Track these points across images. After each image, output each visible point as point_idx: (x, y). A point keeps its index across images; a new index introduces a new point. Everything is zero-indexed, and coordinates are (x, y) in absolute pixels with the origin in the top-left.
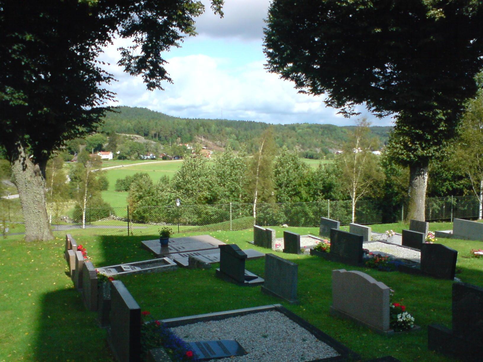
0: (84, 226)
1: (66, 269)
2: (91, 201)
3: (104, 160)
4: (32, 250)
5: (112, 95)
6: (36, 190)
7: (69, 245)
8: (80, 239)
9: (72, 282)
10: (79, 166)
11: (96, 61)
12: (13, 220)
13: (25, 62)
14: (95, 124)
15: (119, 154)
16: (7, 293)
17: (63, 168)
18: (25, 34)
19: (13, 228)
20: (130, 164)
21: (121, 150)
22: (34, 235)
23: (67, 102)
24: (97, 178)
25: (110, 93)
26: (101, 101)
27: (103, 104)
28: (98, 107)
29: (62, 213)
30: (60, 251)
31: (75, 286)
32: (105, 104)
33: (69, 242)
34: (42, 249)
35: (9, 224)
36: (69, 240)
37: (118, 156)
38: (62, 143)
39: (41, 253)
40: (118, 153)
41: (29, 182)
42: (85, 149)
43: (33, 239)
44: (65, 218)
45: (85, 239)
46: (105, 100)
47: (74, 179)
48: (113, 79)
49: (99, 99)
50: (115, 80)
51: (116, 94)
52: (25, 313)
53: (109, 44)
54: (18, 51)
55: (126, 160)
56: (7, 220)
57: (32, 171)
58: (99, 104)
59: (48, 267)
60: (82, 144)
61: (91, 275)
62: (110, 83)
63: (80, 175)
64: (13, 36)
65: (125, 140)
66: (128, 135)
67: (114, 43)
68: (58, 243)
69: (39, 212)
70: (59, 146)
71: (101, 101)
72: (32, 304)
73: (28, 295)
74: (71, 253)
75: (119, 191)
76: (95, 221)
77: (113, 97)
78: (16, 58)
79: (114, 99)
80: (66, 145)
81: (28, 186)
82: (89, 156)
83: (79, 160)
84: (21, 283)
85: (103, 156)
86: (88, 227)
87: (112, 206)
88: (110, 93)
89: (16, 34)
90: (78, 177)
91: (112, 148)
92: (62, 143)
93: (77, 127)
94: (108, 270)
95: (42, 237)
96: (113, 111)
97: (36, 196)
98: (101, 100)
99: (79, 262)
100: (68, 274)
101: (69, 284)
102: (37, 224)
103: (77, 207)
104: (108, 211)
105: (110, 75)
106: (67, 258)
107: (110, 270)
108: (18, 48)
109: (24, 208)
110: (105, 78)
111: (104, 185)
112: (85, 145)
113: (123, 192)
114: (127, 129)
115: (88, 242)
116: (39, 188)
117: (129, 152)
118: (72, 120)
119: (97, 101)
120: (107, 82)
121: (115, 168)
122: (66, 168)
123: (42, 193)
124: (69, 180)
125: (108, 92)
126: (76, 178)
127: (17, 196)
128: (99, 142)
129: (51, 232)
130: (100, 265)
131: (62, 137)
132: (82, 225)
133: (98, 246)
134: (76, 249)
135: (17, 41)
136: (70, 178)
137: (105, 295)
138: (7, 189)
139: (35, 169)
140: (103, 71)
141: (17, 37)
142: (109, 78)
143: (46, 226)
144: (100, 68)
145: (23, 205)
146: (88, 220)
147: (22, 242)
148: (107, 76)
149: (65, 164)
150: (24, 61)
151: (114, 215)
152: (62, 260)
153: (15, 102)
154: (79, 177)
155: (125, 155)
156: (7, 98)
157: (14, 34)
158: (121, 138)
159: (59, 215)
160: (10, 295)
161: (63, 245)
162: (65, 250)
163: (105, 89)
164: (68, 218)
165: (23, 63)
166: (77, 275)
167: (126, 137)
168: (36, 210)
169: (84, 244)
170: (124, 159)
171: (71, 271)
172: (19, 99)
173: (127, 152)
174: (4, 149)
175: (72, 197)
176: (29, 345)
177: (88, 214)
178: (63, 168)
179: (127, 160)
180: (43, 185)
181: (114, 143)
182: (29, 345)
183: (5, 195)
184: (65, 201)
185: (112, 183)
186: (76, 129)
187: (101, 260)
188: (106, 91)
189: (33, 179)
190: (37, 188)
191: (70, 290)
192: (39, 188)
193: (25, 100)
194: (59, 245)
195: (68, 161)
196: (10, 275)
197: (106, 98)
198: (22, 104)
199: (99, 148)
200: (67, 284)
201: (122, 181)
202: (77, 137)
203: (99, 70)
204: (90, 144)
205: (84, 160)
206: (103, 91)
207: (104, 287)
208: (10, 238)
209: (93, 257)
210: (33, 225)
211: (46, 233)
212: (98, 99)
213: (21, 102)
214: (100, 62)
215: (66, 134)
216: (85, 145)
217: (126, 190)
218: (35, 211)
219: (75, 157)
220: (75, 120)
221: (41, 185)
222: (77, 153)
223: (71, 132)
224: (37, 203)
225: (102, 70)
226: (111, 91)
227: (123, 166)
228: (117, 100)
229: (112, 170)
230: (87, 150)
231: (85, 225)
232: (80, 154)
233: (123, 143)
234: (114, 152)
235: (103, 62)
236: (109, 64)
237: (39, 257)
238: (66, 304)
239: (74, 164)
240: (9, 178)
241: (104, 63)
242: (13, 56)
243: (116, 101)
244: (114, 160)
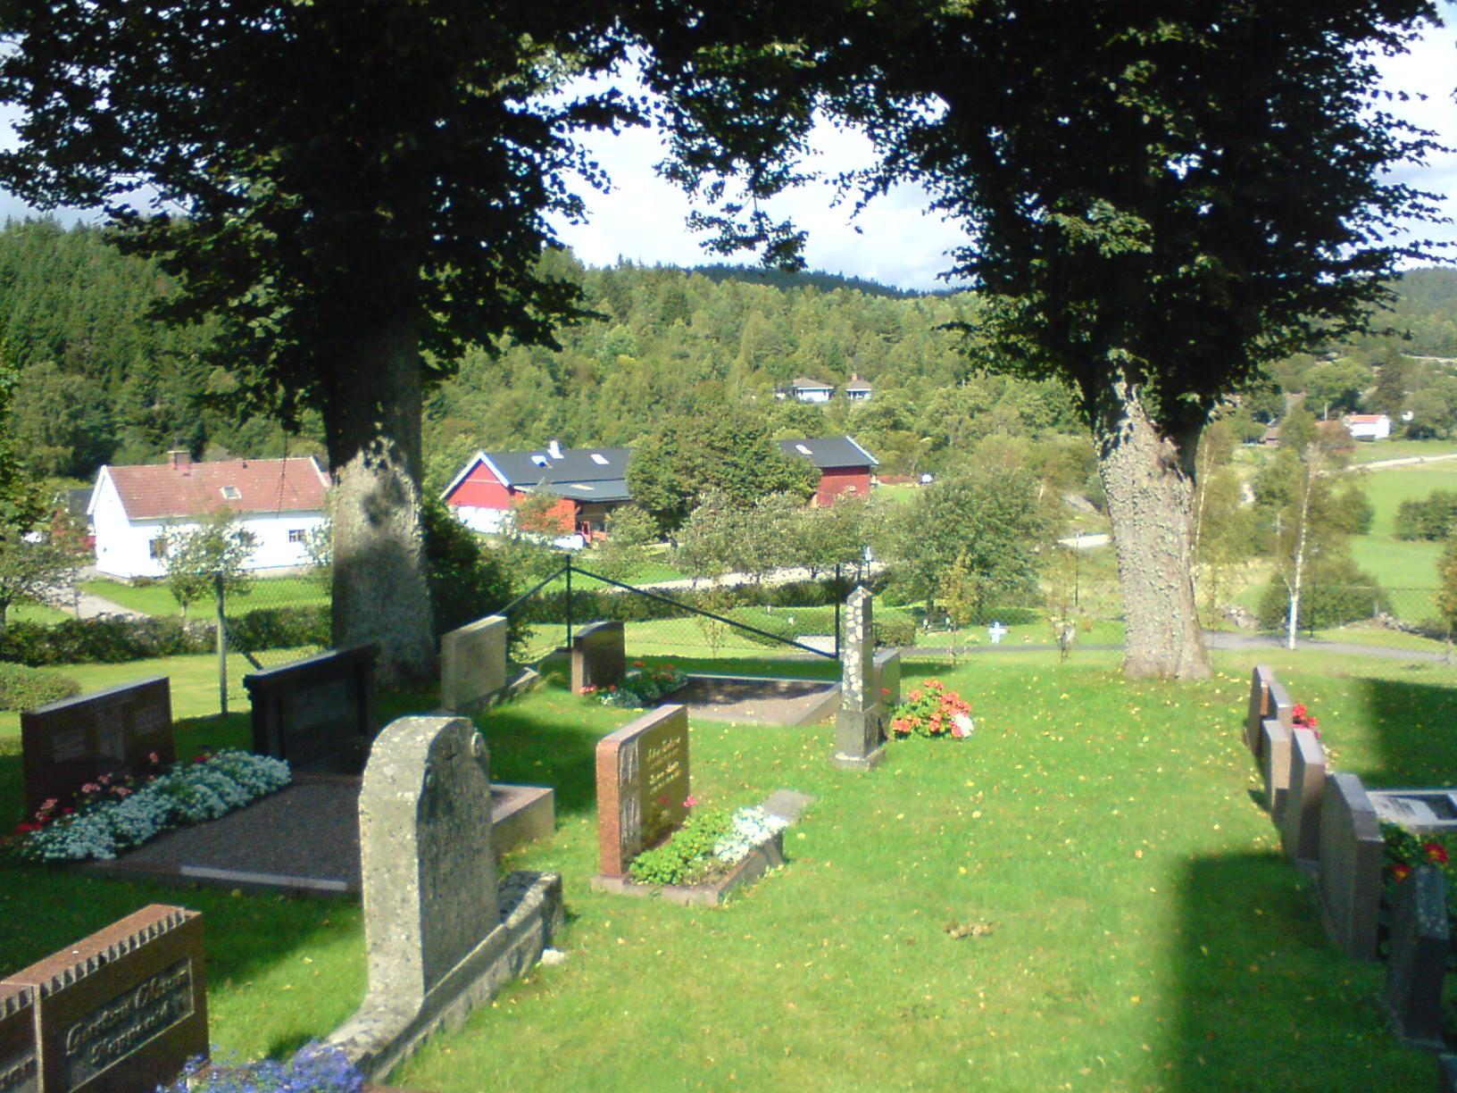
0: (1292, 639)
1: (1252, 779)
2: (1320, 565)
3: (1362, 439)
4: (1145, 704)
5: (1428, 203)
6: (1164, 520)
7: (1265, 703)
8: (1296, 685)
9: (1273, 829)
10: (1287, 458)
11: (1375, 94)
12: (1089, 609)
13: (1152, 116)
14: (1361, 305)
15: (1410, 423)
16: (1074, 835)
17: (1230, 460)
18: (1157, 26)
19: (1088, 630)
20: (1446, 453)
21: (1418, 408)
22: (1151, 659)
23: (1271, 237)
24: (1337, 492)
25: (1420, 196)
26: (1389, 225)
27: (1394, 233)
28: (1378, 245)
29: (1228, 595)
30: (1229, 716)
31: (1284, 846)
32: (1401, 234)
33: (1265, 692)
34: (1173, 703)
35: (1077, 618)
36: (1263, 685)
37: (1406, 428)
38: (1251, 371)
39: (1170, 718)
40: (1408, 417)
41: (1143, 492)
42: (1302, 406)
43: (1147, 669)
44: (1233, 611)
45: (1311, 686)
46: (1401, 222)
47: (1266, 496)
48: (1435, 146)
49: (1382, 220)
50: (1445, 150)
51: (1443, 197)
52: (1126, 916)
53: (1429, 27)
54: (1135, 83)
55: (1433, 442)
56: (1071, 607)
57: (1155, 459)
58: (1379, 238)
59: (1193, 764)
60: (1294, 391)
61: (1357, 823)
62: (1423, 159)
63: (1286, 485)
64: (1124, 38)
65: (1434, 378)
66: (1442, 361)
67: (1444, 22)
68: (1224, 692)
69: (1171, 587)
70: (1241, 382)
71: (1389, 225)
72: (1146, 887)
73: (1133, 856)
74: (1276, 731)
75: (1405, 538)
76: (1327, 628)
77: (1432, 210)
78: (1129, 104)
79: (1437, 215)
80: (1265, 377)
81: (1140, 505)
82: (1315, 428)
83: (1283, 441)
84: (1112, 809)
85: (1358, 426)
86: (1306, 647)
87: (1383, 583)
88: (1420, 196)
89: (1132, 31)
90: (1277, 491)
91: (1389, 401)
92: (1251, 371)
93: (1302, 317)
94: (1400, 805)
95: (1177, 667)
96: (1430, 256)
97: (1163, 538)
98: (1386, 221)
99: (1306, 768)
100: (1260, 798)
101: (1265, 837)
102: (1163, 624)
103: (1278, 579)
104: (1369, 601)
105: (1424, 133)
106: (1261, 747)
107: (1408, 807)
108: (1137, 74)
109: (1123, 572)
110: (1405, 146)
111: (1357, 518)
112: (1304, 394)
113: (1418, 542)
114: (1439, 342)
115: (1323, 696)
116: (1173, 511)
117: (1443, 416)
118: (1285, 295)
119: (1376, 226)
120: (1411, 159)
121: (1396, 465)
122: (1242, 462)
123: (1183, 528)
124: (1251, 499)
125: (1414, 194)
126: (1271, 494)
127: (1101, 540)
128: (1348, 384)
129: (1203, 654)
130: (1372, 781)
131: (1253, 351)
132: (1285, 636)
133: (1355, 714)
134: (1290, 716)
135: (1132, 52)
136: (1255, 494)
137: (1423, 919)
138: (1072, 518)
139: (1164, 454)
140: (1400, 124)
141: (1134, 39)
142: (1418, 145)
143: (1189, 632)
144: (1389, 116)
145: (1123, 562)
146: (1308, 623)
147: (1117, 676)
148: (1413, 138)
149: (1240, 451)
150: (1148, 113)
151: (1390, 615)
152: (1239, 749)
153: (1113, 245)
154: (1282, 491)
155: (1429, 425)
156: (1091, 233)
157: (1126, 33)
158: (1420, 370)
159: (1218, 601)
160: (1081, 842)
161: (1241, 699)
162: (1246, 716)
163: (1403, 186)
164: (1243, 612)
165: (1146, 119)
166: (1294, 815)
167: (1438, 366)
168: (1161, 581)
169: (1310, 703)
170: (1426, 437)
171: (1274, 793)
172: (1127, 233)
173: (1438, 416)
174: (1078, 391)
175: (1261, 551)
176: (1145, 1047)
177: (1308, 607)
178: (1230, 460)
179: (1436, 441)
180: (1186, 503)
181: (1395, 385)
182: (1145, 1047)
183: (1068, 535)
184: (1236, 561)
185: (1385, 508)
186: (1298, 322)
187: (1370, 763)
188: (1407, 190)
189: (1156, 483)
190: (1167, 514)
191: (1268, 858)
192: (1173, 511)
193: (1143, 237)
194: (1226, 698)
195: (1250, 440)
196: (1082, 778)
197: (1407, 215)
198: (1135, 248)
199: (1348, 402)
200: (1257, 834)
201: (1417, 506)
202: (1298, 350)
203: (1386, 120)
204: (1320, 391)
205: (1298, 438)
206: (1396, 194)
207: (1420, 884)
208: (1079, 659)
209: (1340, 749)
210: (1151, 628)
211: (1188, 656)
212: (1376, 218)
213: (1131, 243)
214: (1389, 95)
215: (1261, 341)
216: (1304, 394)
217: (1431, 537)
218: (1160, 584)
219: (1271, 430)
220: (1294, 296)
221: (1181, 503)
222: (1276, 416)
223: (1279, 334)
224: (1164, 559)
225: (1394, 121)
226: (1426, 191)
227: (1422, 461)
228: (1447, 216)
229: (1387, 471)
230: (1308, 408)
231: (1298, 638)
232: (1286, 420)
233: (1425, 385)
234: (1393, 413)
235: (1401, 93)
236: (1424, 97)
237: (1164, 729)
238: (1259, 912)
239: (1267, 450)
240: (1080, 489)
241: (1404, 97)
242: (1121, 99)
243: (1444, 220)
244: (1393, 440)
